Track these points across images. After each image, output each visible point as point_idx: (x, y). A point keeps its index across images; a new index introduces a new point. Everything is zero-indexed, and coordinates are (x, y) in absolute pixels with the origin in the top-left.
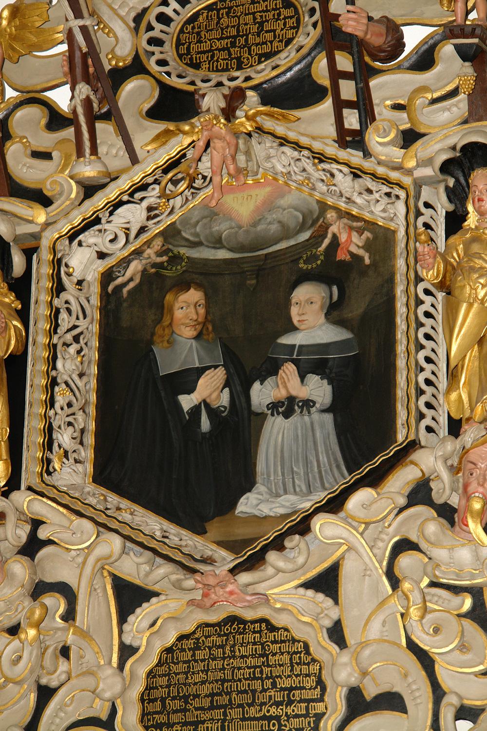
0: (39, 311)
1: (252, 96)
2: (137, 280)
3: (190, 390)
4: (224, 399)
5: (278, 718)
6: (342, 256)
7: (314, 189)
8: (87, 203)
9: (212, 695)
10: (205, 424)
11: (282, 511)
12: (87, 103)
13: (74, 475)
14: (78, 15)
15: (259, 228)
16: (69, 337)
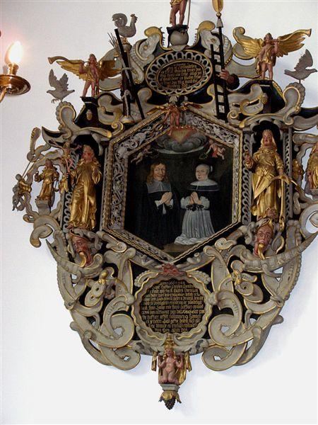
0: (107, 169)
1: (186, 98)
2: (141, 159)
3: (159, 199)
4: (171, 203)
5: (188, 314)
6: (214, 156)
7: (205, 131)
8: (126, 132)
9: (165, 305)
10: (164, 211)
11: (191, 243)
12: (128, 97)
13: (117, 226)
14: (127, 66)
15: (186, 144)
16: (117, 178)
